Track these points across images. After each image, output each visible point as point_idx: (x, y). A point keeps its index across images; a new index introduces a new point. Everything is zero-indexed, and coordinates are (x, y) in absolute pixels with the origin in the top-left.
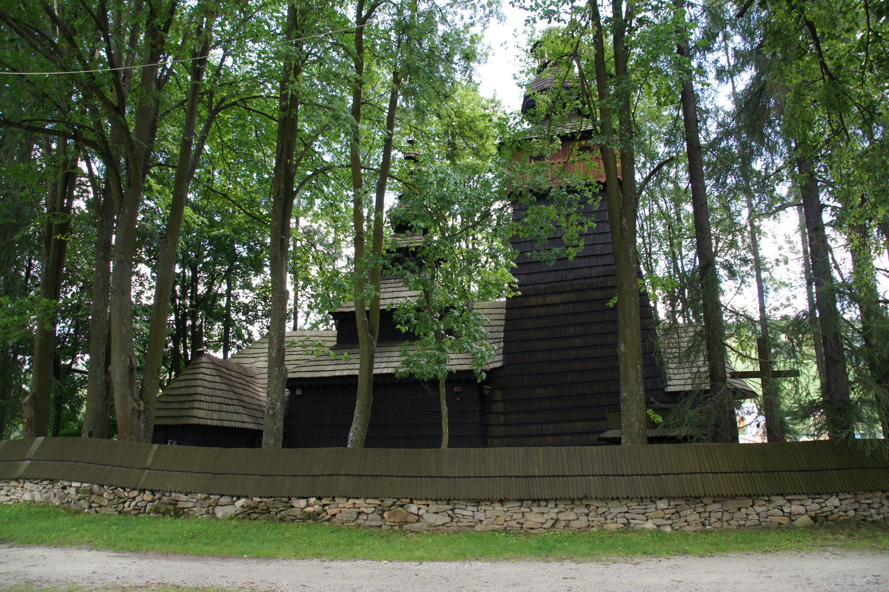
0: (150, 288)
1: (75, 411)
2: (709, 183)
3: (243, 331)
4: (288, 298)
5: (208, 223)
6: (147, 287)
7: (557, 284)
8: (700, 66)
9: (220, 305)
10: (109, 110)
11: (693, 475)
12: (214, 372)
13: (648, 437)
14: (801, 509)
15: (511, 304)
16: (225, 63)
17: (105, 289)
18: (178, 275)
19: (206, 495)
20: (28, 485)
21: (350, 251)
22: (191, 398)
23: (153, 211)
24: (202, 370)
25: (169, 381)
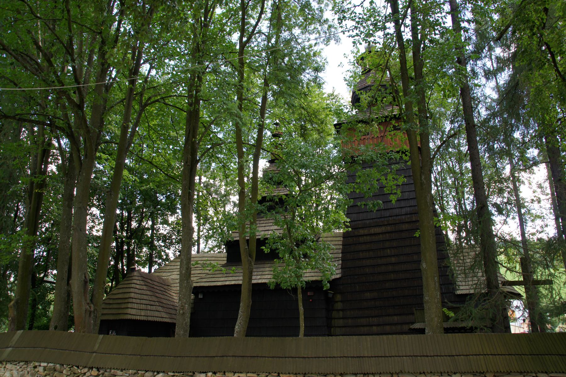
0: (99, 224)
1: (45, 309)
2: (481, 148)
3: (163, 253)
4: (193, 232)
5: (138, 181)
6: (97, 223)
7: (378, 220)
8: (473, 70)
9: (147, 235)
10: (73, 107)
11: (478, 357)
12: (142, 283)
13: (444, 328)
15: (345, 236)
16: (151, 74)
17: (69, 227)
18: (118, 215)
19: (135, 371)
20: (9, 366)
21: (235, 198)
22: (126, 301)
23: (102, 172)
24: (134, 281)
25: (111, 287)
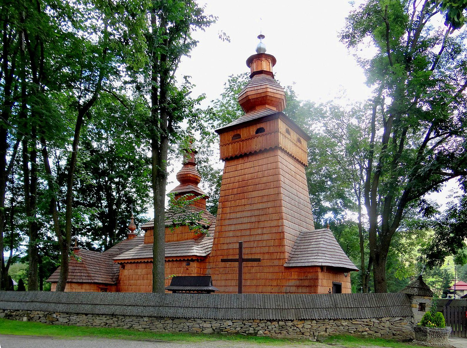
14: (209, 326)
